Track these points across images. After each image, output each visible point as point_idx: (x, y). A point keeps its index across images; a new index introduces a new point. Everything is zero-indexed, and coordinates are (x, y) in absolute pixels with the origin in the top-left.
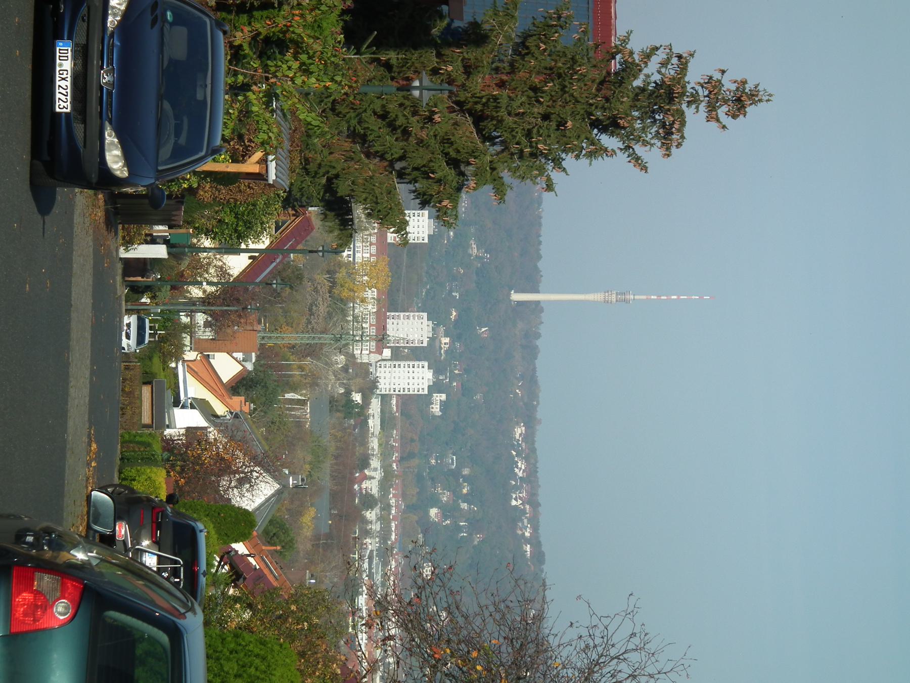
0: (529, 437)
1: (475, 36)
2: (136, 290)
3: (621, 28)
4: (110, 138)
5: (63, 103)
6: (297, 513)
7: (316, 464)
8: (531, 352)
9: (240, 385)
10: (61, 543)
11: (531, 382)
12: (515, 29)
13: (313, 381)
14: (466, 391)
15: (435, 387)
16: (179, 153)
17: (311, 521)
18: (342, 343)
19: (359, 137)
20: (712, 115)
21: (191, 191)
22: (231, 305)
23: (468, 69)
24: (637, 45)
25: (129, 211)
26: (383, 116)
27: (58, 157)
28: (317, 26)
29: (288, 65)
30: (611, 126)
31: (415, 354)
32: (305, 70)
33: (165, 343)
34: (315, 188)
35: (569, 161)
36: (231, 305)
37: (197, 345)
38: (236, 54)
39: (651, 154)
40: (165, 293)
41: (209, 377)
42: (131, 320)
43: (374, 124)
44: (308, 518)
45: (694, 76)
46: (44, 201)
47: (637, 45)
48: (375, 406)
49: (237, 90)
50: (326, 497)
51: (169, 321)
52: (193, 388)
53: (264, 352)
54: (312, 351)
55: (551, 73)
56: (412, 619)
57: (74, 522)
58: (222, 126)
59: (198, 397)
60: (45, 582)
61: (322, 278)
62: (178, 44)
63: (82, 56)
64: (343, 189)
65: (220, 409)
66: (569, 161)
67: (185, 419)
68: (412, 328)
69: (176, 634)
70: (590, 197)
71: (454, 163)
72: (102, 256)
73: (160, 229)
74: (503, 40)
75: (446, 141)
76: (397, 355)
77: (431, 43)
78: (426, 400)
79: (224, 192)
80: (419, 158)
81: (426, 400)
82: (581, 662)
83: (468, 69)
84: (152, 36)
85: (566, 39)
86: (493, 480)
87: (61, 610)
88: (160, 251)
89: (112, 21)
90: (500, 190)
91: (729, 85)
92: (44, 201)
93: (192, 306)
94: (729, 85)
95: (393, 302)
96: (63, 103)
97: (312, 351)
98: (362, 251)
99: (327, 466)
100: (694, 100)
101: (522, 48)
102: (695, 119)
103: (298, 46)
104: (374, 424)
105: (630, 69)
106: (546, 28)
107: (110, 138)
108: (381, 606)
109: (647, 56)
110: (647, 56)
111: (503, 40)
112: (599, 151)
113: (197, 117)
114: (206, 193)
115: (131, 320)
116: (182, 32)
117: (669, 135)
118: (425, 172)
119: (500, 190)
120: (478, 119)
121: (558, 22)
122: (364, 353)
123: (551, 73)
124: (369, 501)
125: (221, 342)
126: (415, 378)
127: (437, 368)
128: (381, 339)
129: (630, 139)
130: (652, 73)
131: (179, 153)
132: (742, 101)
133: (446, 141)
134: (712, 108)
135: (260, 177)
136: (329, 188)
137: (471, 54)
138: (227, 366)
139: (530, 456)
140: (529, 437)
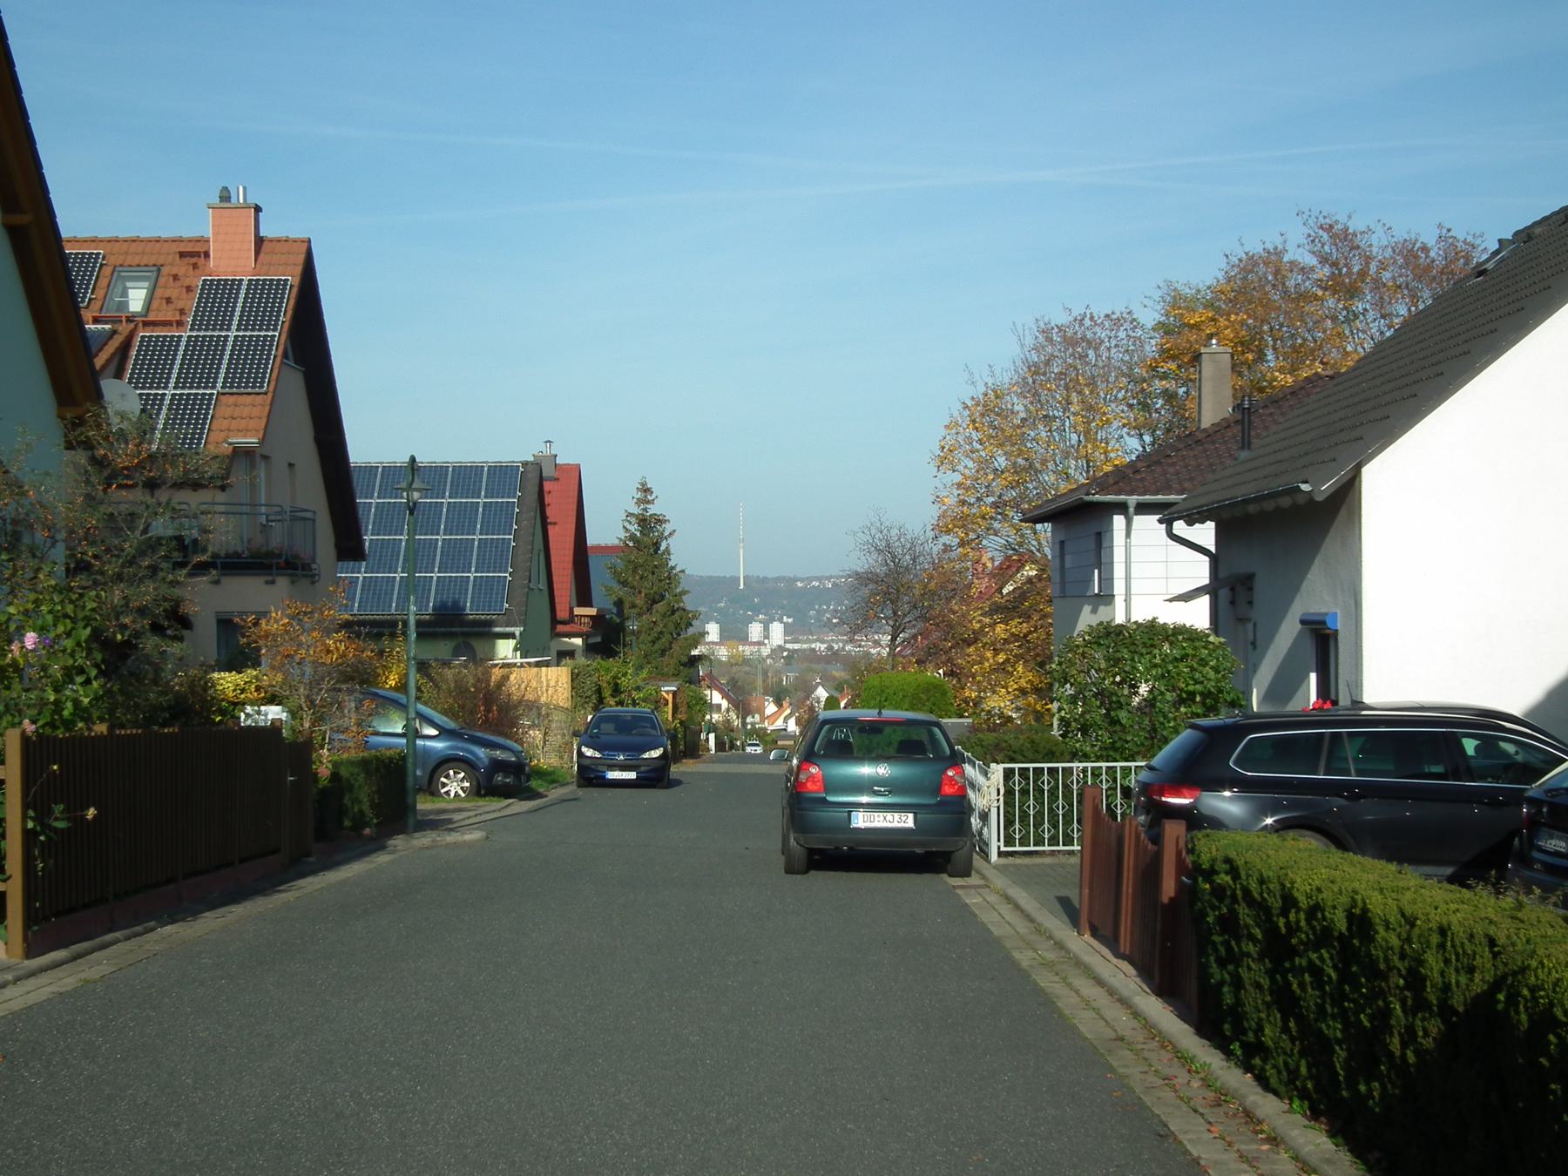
0: (802, 580)
1: (619, 603)
2: (732, 746)
3: (616, 542)
4: (646, 755)
5: (632, 775)
6: (834, 678)
7: (814, 671)
8: (765, 580)
9: (779, 703)
10: (790, 770)
11: (778, 579)
12: (617, 587)
13: (778, 672)
14: (782, 608)
15: (781, 621)
16: (654, 727)
17: (839, 673)
18: (762, 660)
19: (663, 652)
20: (652, 502)
21: (682, 723)
22: (743, 708)
23: (633, 606)
24: (623, 535)
25: (693, 749)
26: (654, 642)
27: (655, 778)
28: (608, 670)
29: (623, 682)
30: (657, 545)
31: (766, 629)
32: (625, 675)
33: (760, 735)
34: (685, 671)
35: (671, 563)
36: (743, 708)
37: (762, 721)
38: (620, 703)
39: (668, 528)
40: (734, 735)
41: (775, 716)
42: (749, 749)
43: (657, 646)
44: (837, 674)
45: (636, 510)
46: (678, 783)
47: (623, 535)
48: (789, 646)
49: (634, 704)
50: (829, 667)
51: (750, 734)
52: (779, 723)
53: (766, 693)
54: (765, 673)
55: (635, 571)
56: (856, 630)
57: (781, 769)
58: (645, 709)
59: (781, 720)
60: (803, 777)
61: (734, 669)
62: (608, 727)
63: (613, 767)
64: (685, 659)
65: (788, 711)
66: (671, 563)
67: (792, 726)
68: (755, 631)
69: (825, 722)
70: (686, 554)
71: (673, 612)
72: (713, 760)
73: (703, 736)
74: (621, 592)
75: (664, 616)
76: (767, 637)
77: (622, 623)
78: (786, 624)
79: (683, 709)
80: (671, 627)
81: (786, 624)
82: (875, 555)
83: (633, 606)
84: (604, 738)
85: (620, 564)
86: (820, 594)
87: (814, 770)
88: (712, 736)
89: (597, 755)
90: (684, 592)
91: (639, 495)
92: (678, 783)
93: (744, 724)
94: (639, 495)
95: (744, 639)
96: (632, 775)
97: (765, 673)
98: (723, 653)
99: (815, 666)
100: (645, 510)
101: (624, 583)
102: (653, 509)
103: (615, 677)
104: (796, 646)
105: (632, 537)
106: (616, 574)
107: (646, 755)
108: (851, 641)
109: (627, 530)
110: (627, 530)
111: (621, 592)
112: (667, 551)
113: (638, 720)
114: (683, 717)
115: (749, 749)
116: (603, 726)
117: (660, 521)
118: (677, 625)
119: (684, 592)
120: (655, 602)
121: (613, 568)
122: (766, 651)
123: (635, 571)
124: (830, 648)
125: (761, 711)
126: (777, 630)
127: (772, 620)
128: (759, 643)
129: (662, 537)
130: (634, 528)
131: (654, 727)
132: (646, 490)
133: (664, 616)
134: (648, 502)
135: (674, 694)
136: (684, 665)
137: (627, 605)
138: (771, 708)
139: (810, 579)
140: (802, 580)
